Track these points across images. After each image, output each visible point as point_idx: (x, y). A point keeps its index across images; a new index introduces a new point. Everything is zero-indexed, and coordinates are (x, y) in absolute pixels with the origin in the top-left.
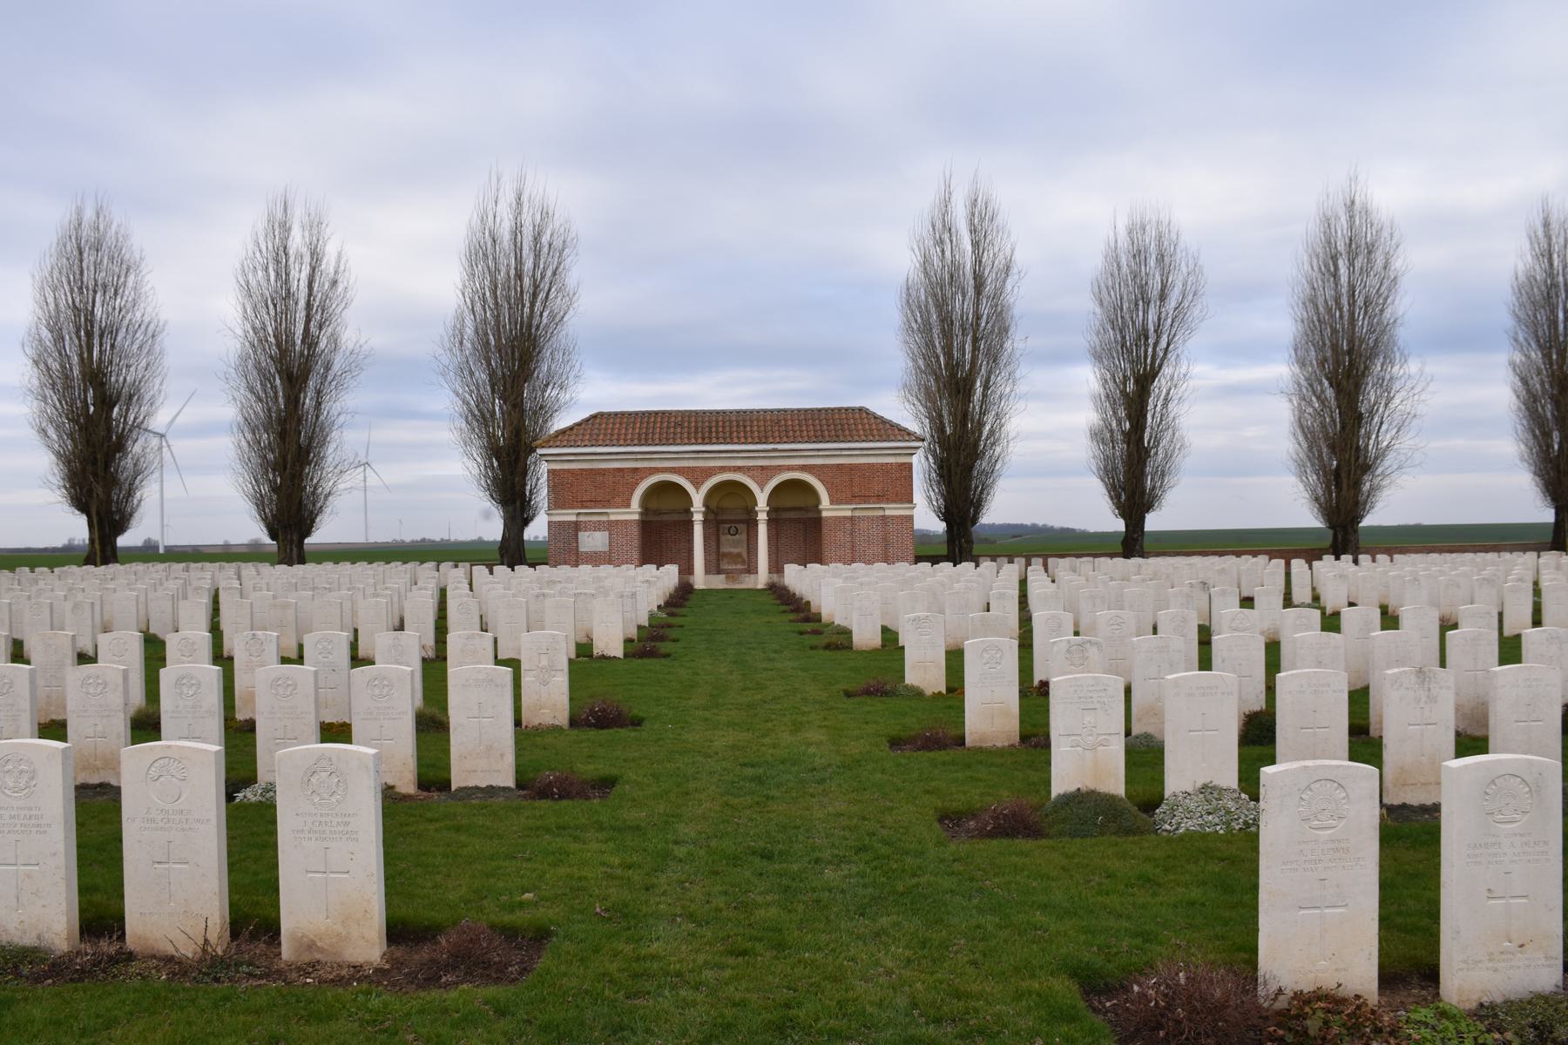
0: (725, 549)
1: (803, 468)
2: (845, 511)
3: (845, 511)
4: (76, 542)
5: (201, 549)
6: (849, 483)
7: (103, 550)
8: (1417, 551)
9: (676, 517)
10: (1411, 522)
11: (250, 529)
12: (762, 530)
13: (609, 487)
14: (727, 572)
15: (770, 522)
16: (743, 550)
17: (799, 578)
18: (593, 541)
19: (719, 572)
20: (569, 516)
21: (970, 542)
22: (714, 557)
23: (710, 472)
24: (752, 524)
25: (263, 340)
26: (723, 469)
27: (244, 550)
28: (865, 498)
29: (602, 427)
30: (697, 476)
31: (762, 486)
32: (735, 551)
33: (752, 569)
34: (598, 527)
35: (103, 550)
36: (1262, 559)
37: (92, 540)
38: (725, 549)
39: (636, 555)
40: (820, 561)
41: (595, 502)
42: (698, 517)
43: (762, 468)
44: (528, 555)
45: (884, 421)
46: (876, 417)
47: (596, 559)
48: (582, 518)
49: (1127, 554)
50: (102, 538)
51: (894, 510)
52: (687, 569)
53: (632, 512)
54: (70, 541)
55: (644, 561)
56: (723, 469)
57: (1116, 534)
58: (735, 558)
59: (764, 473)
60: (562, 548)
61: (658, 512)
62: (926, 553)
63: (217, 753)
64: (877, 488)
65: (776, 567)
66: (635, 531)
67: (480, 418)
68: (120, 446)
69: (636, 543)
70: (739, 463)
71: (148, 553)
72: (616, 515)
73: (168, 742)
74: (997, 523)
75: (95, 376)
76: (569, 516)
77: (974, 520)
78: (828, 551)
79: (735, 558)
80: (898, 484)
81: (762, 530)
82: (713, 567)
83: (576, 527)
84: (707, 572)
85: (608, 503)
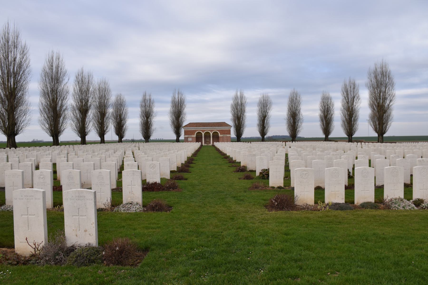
0: (207, 140)
1: (217, 130)
2: (222, 136)
3: (222, 136)
4: (35, 140)
5: (69, 142)
6: (222, 132)
7: (120, 141)
8: (306, 141)
9: (200, 136)
10: (392, 135)
11: (140, 137)
12: (211, 138)
13: (192, 133)
14: (207, 144)
15: (212, 137)
16: (209, 141)
17: (217, 144)
18: (190, 139)
19: (206, 143)
20: (187, 136)
21: (240, 140)
22: (205, 141)
23: (205, 131)
24: (210, 137)
25: (143, 112)
26: (206, 130)
27: (74, 142)
28: (224, 134)
29: (191, 125)
30: (203, 131)
31: (211, 133)
32: (208, 141)
33: (210, 143)
34: (190, 138)
36: (282, 142)
37: (119, 139)
38: (207, 140)
39: (195, 141)
40: (219, 142)
42: (203, 136)
44: (180, 141)
45: (227, 124)
46: (226, 123)
47: (190, 142)
49: (325, 141)
50: (120, 139)
51: (228, 135)
52: (202, 143)
53: (195, 136)
54: (34, 140)
55: (196, 142)
56: (206, 130)
57: (377, 137)
58: (208, 142)
59: (211, 131)
60: (186, 140)
61: (198, 136)
62: (232, 141)
63: (51, 172)
65: (213, 143)
66: (195, 138)
67: (173, 122)
68: (123, 126)
69: (195, 140)
71: (127, 141)
72: (193, 136)
73: (41, 170)
74: (3, 141)
75: (120, 116)
76: (187, 136)
77: (241, 137)
79: (208, 142)
80: (229, 132)
81: (211, 138)
82: (205, 143)
83: (188, 138)
84: (204, 143)
85: (192, 134)
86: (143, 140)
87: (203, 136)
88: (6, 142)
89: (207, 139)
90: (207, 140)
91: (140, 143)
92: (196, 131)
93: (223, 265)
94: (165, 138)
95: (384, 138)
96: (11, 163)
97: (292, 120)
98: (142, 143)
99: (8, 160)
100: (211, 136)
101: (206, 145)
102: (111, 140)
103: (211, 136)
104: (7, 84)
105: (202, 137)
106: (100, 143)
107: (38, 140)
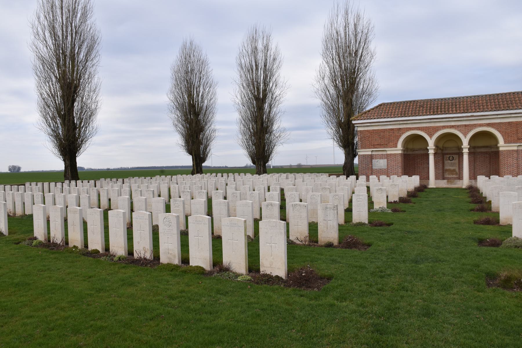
0: (447, 167)
1: (489, 125)
2: (513, 147)
3: (513, 147)
11: (246, 161)
14: (448, 179)
15: (470, 154)
18: (380, 164)
23: (437, 129)
24: (460, 155)
26: (444, 127)
30: (431, 131)
32: (452, 168)
33: (460, 178)
34: (381, 157)
35: (197, 169)
38: (447, 167)
41: (380, 145)
42: (431, 152)
43: (465, 126)
48: (374, 153)
52: (425, 177)
53: (398, 149)
56: (444, 127)
58: (452, 172)
59: (466, 128)
65: (473, 176)
66: (400, 159)
70: (453, 124)
72: (390, 151)
78: (502, 169)
79: (452, 172)
82: (441, 175)
83: (371, 157)
84: (437, 178)
85: (386, 145)
86: (251, 167)
87: (431, 152)
88: (62, 170)
89: (447, 162)
90: (449, 165)
91: (236, 175)
92: (401, 131)
93: (81, 271)
94: (230, 165)
96: (176, 215)
98: (249, 175)
99: (50, 190)
100: (466, 151)
101: (443, 184)
102: (333, 164)
103: (466, 151)
104: (58, 77)
105: (428, 155)
106: (193, 174)
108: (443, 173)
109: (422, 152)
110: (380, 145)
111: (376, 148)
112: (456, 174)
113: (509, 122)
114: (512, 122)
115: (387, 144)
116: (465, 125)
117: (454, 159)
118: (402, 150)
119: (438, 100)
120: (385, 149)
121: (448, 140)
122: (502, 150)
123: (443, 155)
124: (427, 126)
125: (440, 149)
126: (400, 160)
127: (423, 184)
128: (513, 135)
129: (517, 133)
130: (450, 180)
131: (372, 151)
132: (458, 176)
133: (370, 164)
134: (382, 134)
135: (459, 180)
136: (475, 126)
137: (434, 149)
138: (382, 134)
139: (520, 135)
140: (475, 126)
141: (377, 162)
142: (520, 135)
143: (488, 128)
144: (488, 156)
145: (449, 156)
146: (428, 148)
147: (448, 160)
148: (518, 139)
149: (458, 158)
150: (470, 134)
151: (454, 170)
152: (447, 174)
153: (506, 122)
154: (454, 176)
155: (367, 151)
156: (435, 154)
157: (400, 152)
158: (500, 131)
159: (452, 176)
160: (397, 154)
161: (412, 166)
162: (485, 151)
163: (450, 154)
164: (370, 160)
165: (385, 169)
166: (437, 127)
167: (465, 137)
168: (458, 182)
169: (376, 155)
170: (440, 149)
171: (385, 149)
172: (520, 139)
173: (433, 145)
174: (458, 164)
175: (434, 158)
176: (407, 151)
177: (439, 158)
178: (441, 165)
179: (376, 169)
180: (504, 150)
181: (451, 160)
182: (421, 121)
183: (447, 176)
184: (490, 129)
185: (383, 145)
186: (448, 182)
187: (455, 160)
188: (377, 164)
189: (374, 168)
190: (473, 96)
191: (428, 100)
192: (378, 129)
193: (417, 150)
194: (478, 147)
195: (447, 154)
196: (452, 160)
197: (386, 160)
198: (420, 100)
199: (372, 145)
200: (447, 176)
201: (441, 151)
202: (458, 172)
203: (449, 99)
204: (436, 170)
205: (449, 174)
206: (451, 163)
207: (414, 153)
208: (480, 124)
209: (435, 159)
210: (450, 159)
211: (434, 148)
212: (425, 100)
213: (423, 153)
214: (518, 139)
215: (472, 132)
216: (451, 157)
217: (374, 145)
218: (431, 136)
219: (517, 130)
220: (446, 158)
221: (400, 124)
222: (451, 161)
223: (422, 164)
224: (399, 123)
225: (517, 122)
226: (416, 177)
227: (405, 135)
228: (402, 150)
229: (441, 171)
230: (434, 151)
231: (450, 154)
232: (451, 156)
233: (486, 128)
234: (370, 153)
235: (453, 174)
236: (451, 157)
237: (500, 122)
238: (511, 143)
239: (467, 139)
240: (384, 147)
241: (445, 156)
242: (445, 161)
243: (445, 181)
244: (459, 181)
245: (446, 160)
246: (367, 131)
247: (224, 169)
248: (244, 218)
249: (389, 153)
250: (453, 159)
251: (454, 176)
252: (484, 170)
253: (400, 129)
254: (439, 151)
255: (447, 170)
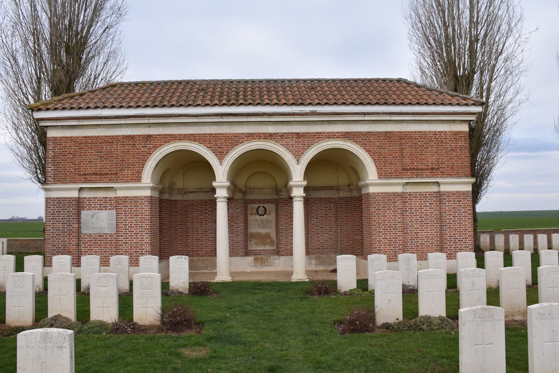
0: (253, 230)
1: (346, 136)
4: (15, 218)
10: (499, 210)
12: (298, 208)
15: (307, 201)
19: (247, 253)
23: (235, 140)
26: (251, 137)
28: (417, 171)
31: (298, 156)
32: (263, 231)
34: (103, 204)
38: (253, 230)
41: (100, 175)
42: (221, 194)
48: (85, 195)
51: (9, 239)
56: (251, 137)
64: (431, 159)
66: (146, 209)
70: (271, 129)
84: (233, 252)
87: (221, 194)
89: (254, 219)
95: (477, 216)
97: (479, 155)
105: (213, 203)
107: (19, 217)
108: (246, 241)
109: (203, 197)
110: (101, 174)
111: (90, 181)
112: (272, 243)
113: (386, 133)
114: (392, 132)
115: (116, 174)
116: (298, 134)
117: (268, 212)
118: (153, 189)
119: (239, 82)
120: (112, 185)
121: (256, 173)
122: (374, 193)
123: (246, 203)
124: (213, 132)
125: (240, 191)
126: (148, 213)
127: (197, 279)
128: (393, 161)
129: (402, 157)
130: (259, 256)
131: (81, 189)
132: (274, 248)
133: (75, 221)
134: (106, 148)
135: (277, 257)
136: (319, 136)
137: (228, 188)
138: (106, 148)
139: (407, 161)
140: (319, 136)
141: (93, 216)
142: (407, 161)
143: (345, 143)
144: (332, 206)
145: (258, 205)
146: (214, 184)
147: (254, 214)
148: (403, 169)
149: (274, 209)
150: (308, 154)
151: (267, 236)
152: (252, 243)
153: (381, 132)
154: (268, 247)
155: (68, 189)
156: (230, 200)
157: (148, 193)
158: (368, 151)
159: (263, 248)
160: (141, 198)
161: (181, 227)
162: (328, 196)
163: (259, 201)
164: (74, 212)
165: (111, 235)
166: (236, 136)
167: (298, 160)
168: (276, 261)
169: (90, 199)
170: (240, 191)
171: (112, 185)
172: (407, 170)
173: (225, 180)
174: (274, 222)
175: (228, 209)
176: (171, 193)
177: (239, 211)
178: (241, 225)
179: (90, 235)
180: (378, 193)
181: (260, 215)
182: (200, 120)
183: (253, 247)
184: (349, 144)
185: (107, 174)
186: (256, 260)
187: (270, 214)
188: (92, 223)
189: (84, 231)
190: (308, 80)
191: (218, 80)
192: (97, 134)
193: (191, 192)
194: (314, 187)
195: (254, 201)
196: (263, 215)
197: (114, 212)
198: (200, 81)
199: (80, 175)
200: (253, 247)
201: (241, 194)
202: (275, 239)
203: (261, 81)
204: (232, 235)
205: (257, 244)
206: (262, 221)
207: (185, 197)
208: (328, 133)
209: (181, 253)
210: (260, 212)
211: (228, 184)
212: (211, 80)
213: (203, 198)
214: (403, 169)
215: (313, 150)
216: (261, 208)
217: (86, 175)
218: (221, 155)
219: (402, 150)
220: (252, 210)
221: (150, 125)
222: (262, 217)
223: (201, 223)
224: (147, 121)
225: (402, 132)
226: (180, 260)
227: (161, 151)
228: (153, 189)
229: (241, 238)
230: (228, 193)
231: (259, 201)
232: (262, 205)
233: (342, 143)
234: (75, 194)
235: (264, 244)
236: (261, 208)
237: (368, 130)
238: (390, 177)
239: (301, 165)
240: (110, 181)
241: (249, 205)
242: (249, 216)
243: (250, 259)
244: (279, 259)
245: (251, 214)
246: (71, 139)
247: (3, 222)
248: (33, 273)
249: (121, 194)
250: (265, 213)
251: (268, 247)
252: (326, 235)
253: (150, 136)
254: (239, 196)
255: (253, 236)
